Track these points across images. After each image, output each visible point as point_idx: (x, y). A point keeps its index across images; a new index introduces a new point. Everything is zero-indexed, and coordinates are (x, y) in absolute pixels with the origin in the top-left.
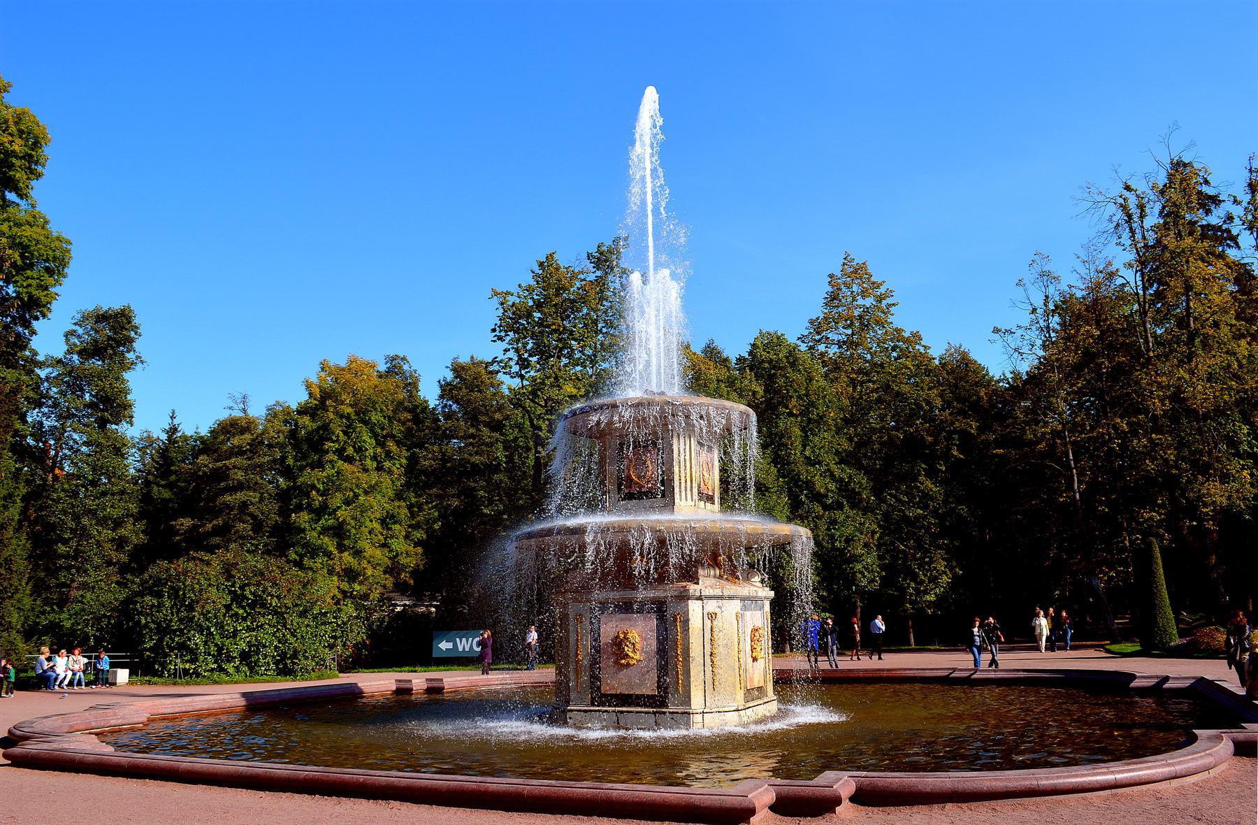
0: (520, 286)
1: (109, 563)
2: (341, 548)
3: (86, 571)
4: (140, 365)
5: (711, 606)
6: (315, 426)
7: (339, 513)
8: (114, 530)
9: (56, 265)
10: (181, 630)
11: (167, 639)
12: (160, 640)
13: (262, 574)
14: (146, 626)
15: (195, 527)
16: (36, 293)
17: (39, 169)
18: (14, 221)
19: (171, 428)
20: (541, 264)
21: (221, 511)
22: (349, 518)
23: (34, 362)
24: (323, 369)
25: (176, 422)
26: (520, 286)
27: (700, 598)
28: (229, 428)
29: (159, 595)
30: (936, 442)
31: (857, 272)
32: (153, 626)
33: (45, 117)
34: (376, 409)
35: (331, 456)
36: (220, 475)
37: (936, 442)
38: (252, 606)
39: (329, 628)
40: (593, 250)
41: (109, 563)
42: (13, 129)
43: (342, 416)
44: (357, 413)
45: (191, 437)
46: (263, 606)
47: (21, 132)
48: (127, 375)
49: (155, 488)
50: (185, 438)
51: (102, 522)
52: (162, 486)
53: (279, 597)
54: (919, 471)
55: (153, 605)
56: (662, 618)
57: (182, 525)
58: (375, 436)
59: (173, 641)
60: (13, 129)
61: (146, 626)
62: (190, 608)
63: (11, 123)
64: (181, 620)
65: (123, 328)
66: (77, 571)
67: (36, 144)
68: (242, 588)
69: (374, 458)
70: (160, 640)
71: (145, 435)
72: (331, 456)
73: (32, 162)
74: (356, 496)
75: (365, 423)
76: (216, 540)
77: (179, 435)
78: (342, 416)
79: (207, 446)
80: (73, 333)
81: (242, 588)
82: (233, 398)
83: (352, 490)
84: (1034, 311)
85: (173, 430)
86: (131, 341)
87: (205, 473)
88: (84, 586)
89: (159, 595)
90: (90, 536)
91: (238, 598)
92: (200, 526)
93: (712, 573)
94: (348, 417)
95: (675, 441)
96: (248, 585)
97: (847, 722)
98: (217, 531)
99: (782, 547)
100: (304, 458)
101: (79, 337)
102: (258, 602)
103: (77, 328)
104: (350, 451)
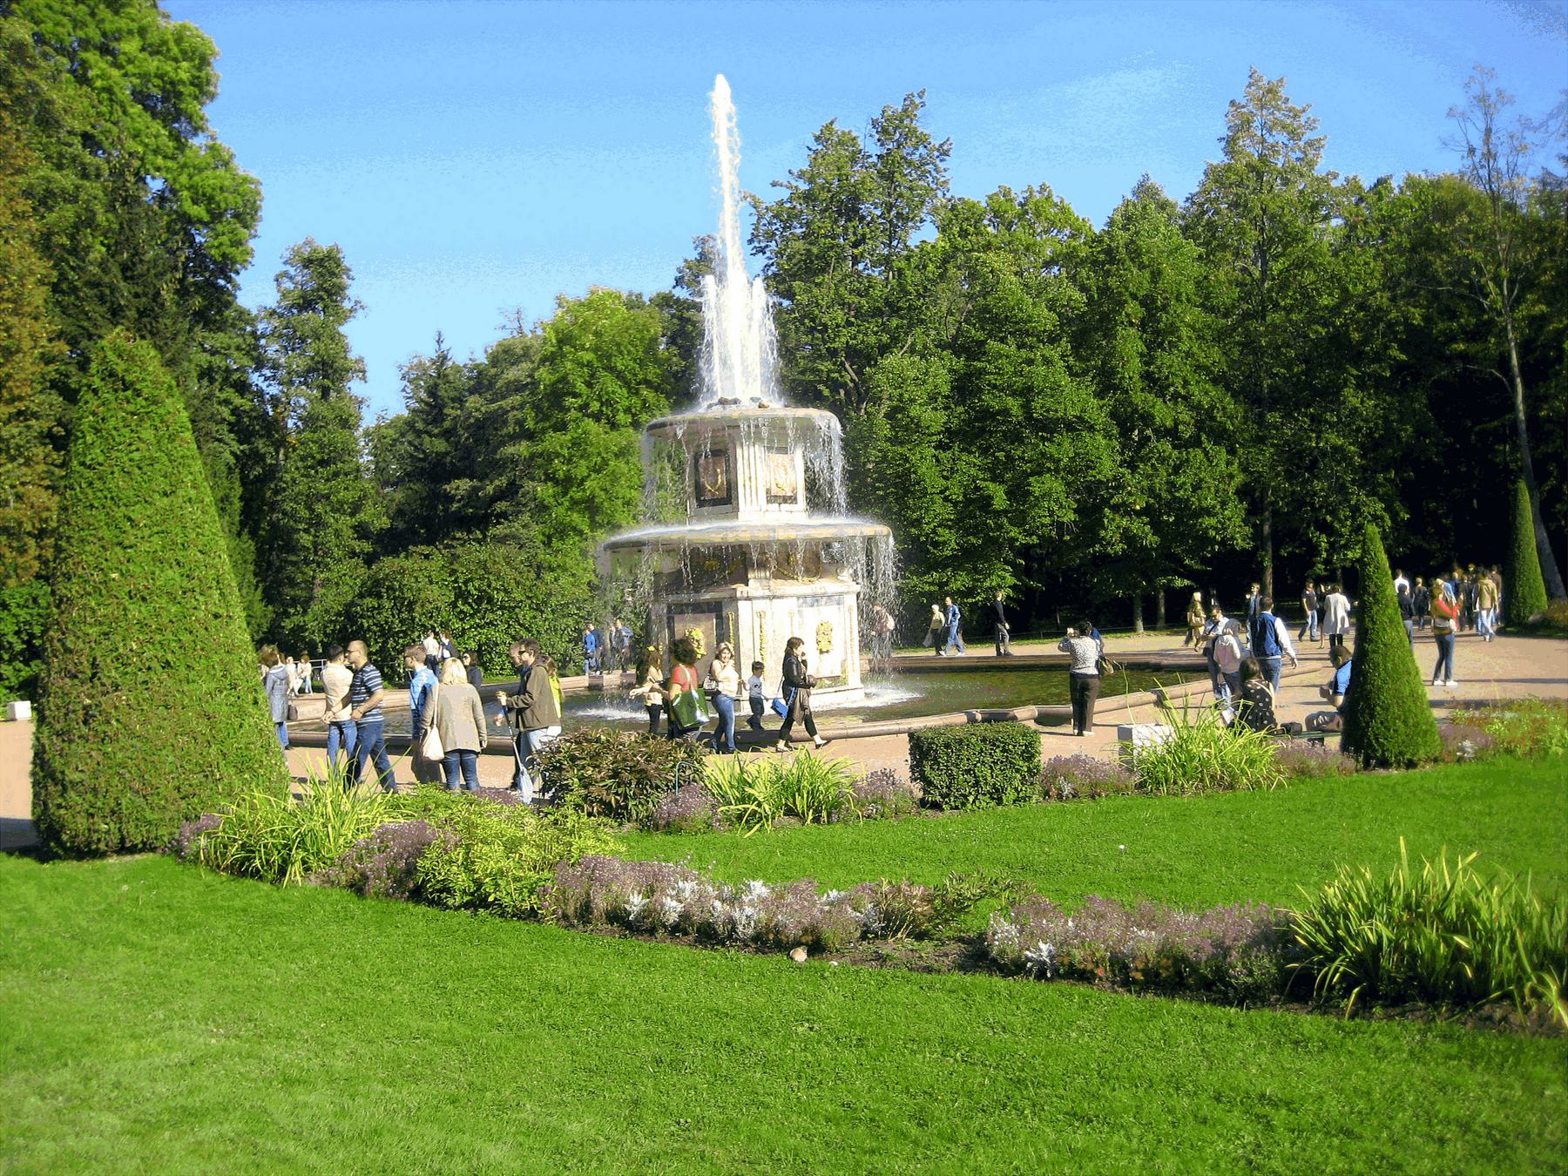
0: (790, 172)
1: (353, 554)
2: (594, 525)
3: (327, 565)
4: (360, 312)
5: (760, 605)
6: (553, 378)
7: (588, 484)
8: (352, 515)
9: (246, 215)
10: (404, 632)
11: (391, 641)
12: (385, 643)
13: (485, 568)
14: (369, 629)
15: (475, 490)
16: (228, 250)
17: (212, 89)
18: (194, 167)
19: (439, 357)
20: (817, 139)
21: (504, 466)
22: (597, 490)
23: (242, 314)
24: (560, 305)
25: (444, 346)
26: (790, 172)
27: (748, 599)
28: (504, 356)
29: (379, 596)
30: (1365, 341)
31: (1269, 95)
32: (374, 628)
33: (211, 31)
34: (621, 353)
35: (573, 414)
36: (497, 419)
37: (1365, 341)
38: (479, 601)
39: (571, 622)
40: (877, 115)
41: (353, 554)
42: (175, 50)
43: (581, 365)
44: (600, 359)
45: (465, 366)
46: (490, 600)
47: (184, 52)
48: (342, 329)
49: (427, 438)
50: (457, 369)
51: (338, 509)
52: (435, 436)
53: (506, 591)
54: (1346, 381)
55: (374, 608)
56: (719, 617)
57: (457, 488)
58: (627, 384)
59: (398, 643)
60: (175, 50)
61: (369, 629)
62: (411, 609)
63: (172, 45)
64: (402, 621)
65: (333, 274)
66: (318, 566)
67: (204, 61)
68: (465, 583)
69: (628, 410)
70: (385, 643)
71: (416, 361)
72: (573, 414)
73: (202, 88)
74: (605, 462)
75: (611, 369)
76: (501, 506)
77: (450, 363)
78: (581, 365)
79: (482, 381)
80: (285, 274)
81: (465, 583)
82: (502, 312)
83: (599, 454)
84: (1472, 151)
85: (443, 358)
86: (342, 288)
87: (477, 420)
88: (326, 583)
89: (379, 596)
90: (326, 525)
91: (461, 595)
92: (480, 489)
93: (763, 574)
94: (589, 364)
95: (739, 451)
96: (471, 580)
97: (923, 700)
98: (500, 495)
99: (870, 541)
100: (546, 418)
101: (291, 278)
102: (485, 598)
103: (288, 268)
104: (595, 406)
